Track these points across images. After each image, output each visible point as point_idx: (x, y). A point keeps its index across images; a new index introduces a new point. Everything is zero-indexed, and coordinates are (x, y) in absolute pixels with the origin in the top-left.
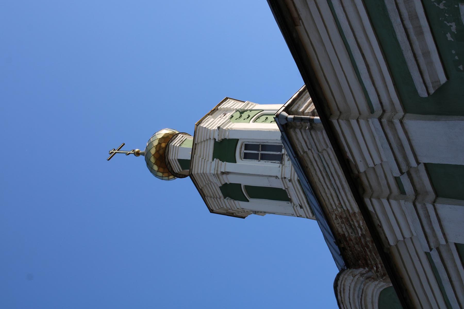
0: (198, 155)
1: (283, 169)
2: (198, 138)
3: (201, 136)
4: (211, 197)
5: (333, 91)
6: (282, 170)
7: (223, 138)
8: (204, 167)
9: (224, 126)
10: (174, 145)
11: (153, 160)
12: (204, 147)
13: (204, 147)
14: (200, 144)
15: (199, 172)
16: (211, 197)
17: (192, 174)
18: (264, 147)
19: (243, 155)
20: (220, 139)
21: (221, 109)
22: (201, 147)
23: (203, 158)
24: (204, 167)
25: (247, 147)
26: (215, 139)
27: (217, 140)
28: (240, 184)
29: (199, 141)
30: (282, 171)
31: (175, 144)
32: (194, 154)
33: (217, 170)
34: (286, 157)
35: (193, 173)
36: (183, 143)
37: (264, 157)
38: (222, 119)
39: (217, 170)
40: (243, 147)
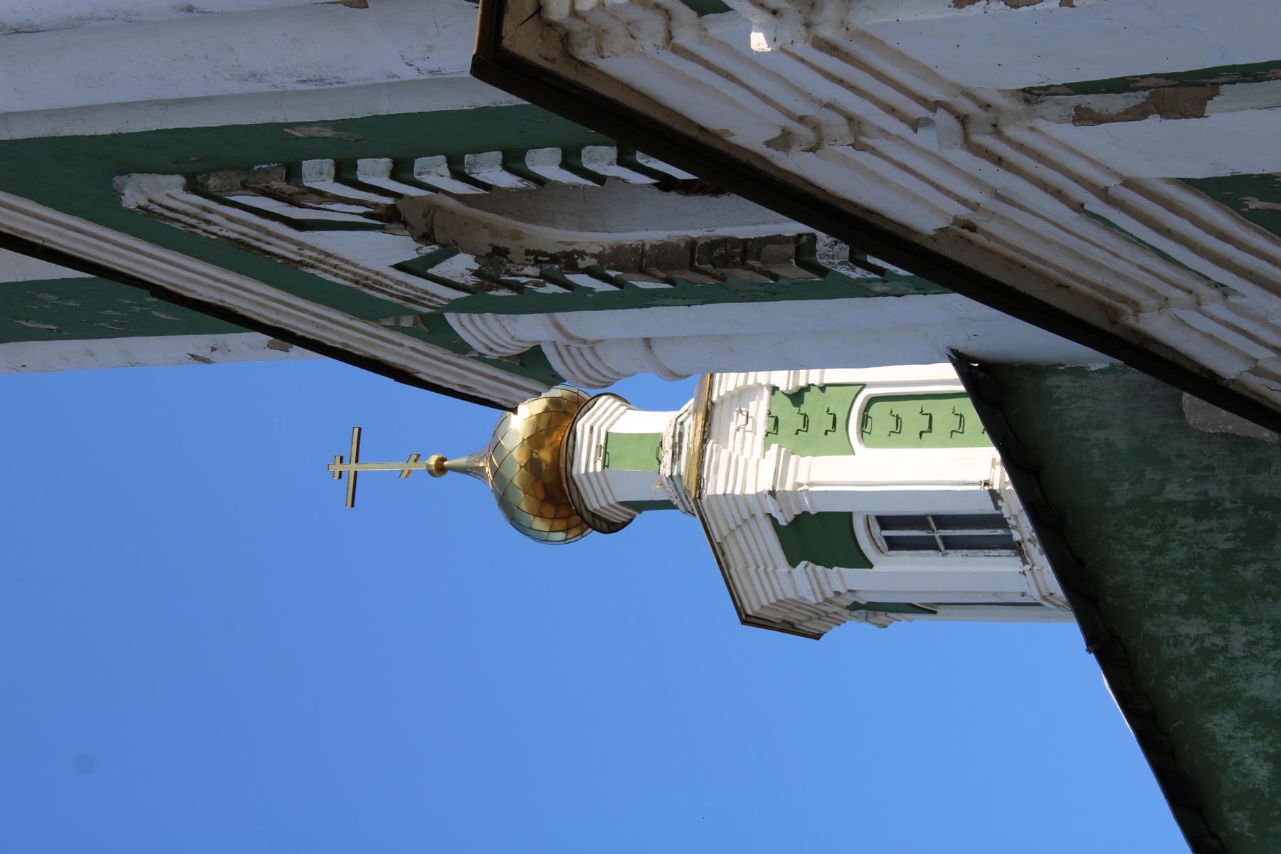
0: (740, 567)
1: (1039, 578)
2: (718, 528)
3: (725, 520)
4: (810, 619)
5: (1034, 218)
6: (1035, 579)
7: (798, 512)
8: (772, 586)
9: (783, 482)
10: (586, 472)
11: (522, 501)
12: (746, 541)
13: (746, 541)
14: (730, 540)
15: (765, 603)
16: (810, 619)
17: (747, 616)
18: (943, 521)
19: (884, 545)
20: (790, 519)
21: (722, 400)
22: (737, 543)
23: (758, 567)
24: (772, 586)
25: (885, 522)
26: (774, 521)
27: (782, 523)
28: (849, 516)
29: (725, 533)
30: (1037, 584)
31: (587, 466)
32: (728, 567)
33: (822, 592)
34: (1030, 546)
35: (749, 612)
36: (606, 452)
37: (952, 544)
38: (749, 436)
39: (822, 592)
40: (875, 527)
